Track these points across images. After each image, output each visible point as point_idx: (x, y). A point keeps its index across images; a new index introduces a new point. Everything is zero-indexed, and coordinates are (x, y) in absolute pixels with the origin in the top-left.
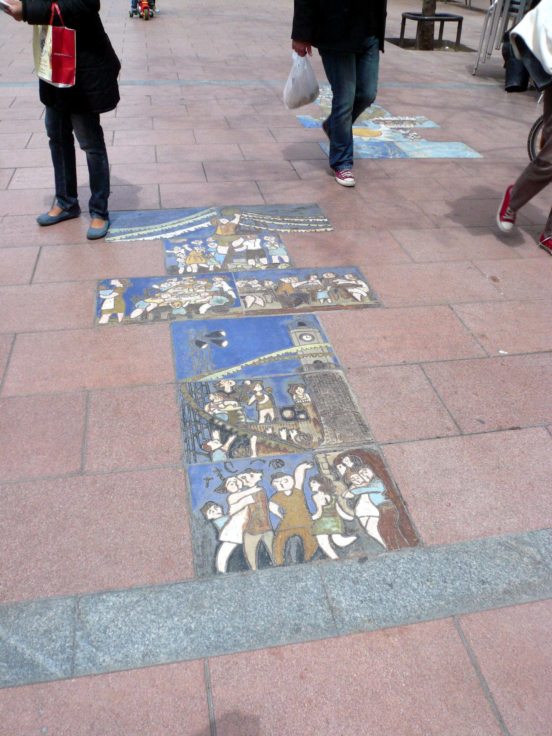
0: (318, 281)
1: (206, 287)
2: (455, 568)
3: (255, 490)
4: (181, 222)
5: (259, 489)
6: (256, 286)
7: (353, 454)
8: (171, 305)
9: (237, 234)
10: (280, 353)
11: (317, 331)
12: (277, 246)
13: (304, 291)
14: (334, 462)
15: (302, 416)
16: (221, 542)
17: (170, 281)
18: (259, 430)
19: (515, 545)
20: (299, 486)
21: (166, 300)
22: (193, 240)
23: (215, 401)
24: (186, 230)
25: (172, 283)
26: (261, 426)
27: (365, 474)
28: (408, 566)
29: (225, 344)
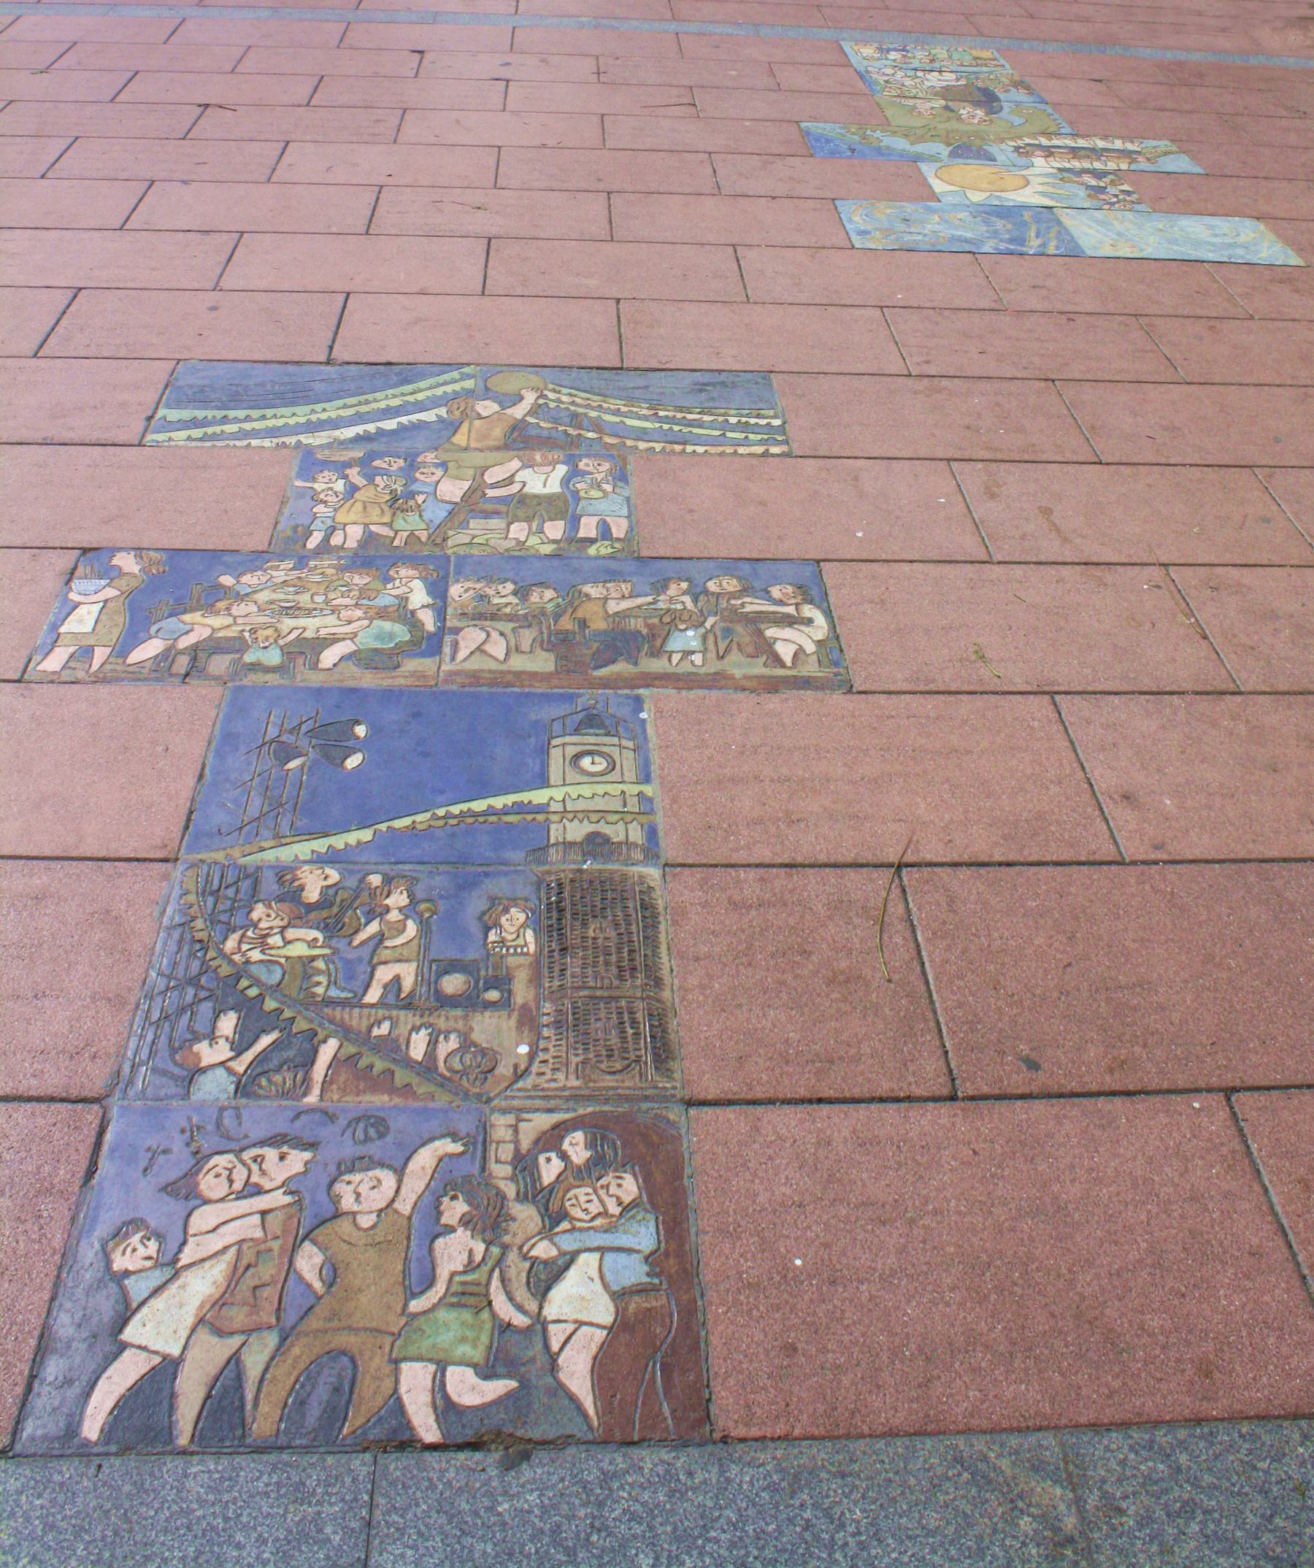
0: (687, 599)
1: (364, 592)
2: (790, 1520)
3: (279, 1199)
4: (367, 402)
5: (288, 1199)
6: (504, 600)
7: (597, 1128)
8: (247, 635)
9: (506, 447)
10: (499, 802)
11: (630, 744)
12: (608, 488)
13: (636, 624)
14: (537, 1141)
15: (493, 995)
16: (124, 1346)
17: (271, 568)
18: (354, 1023)
19: (1009, 1472)
20: (404, 1206)
21: (240, 621)
22: (380, 455)
23: (263, 925)
24: (371, 428)
25: (275, 573)
26: (366, 1011)
27: (613, 1190)
28: (646, 1496)
29: (353, 762)
